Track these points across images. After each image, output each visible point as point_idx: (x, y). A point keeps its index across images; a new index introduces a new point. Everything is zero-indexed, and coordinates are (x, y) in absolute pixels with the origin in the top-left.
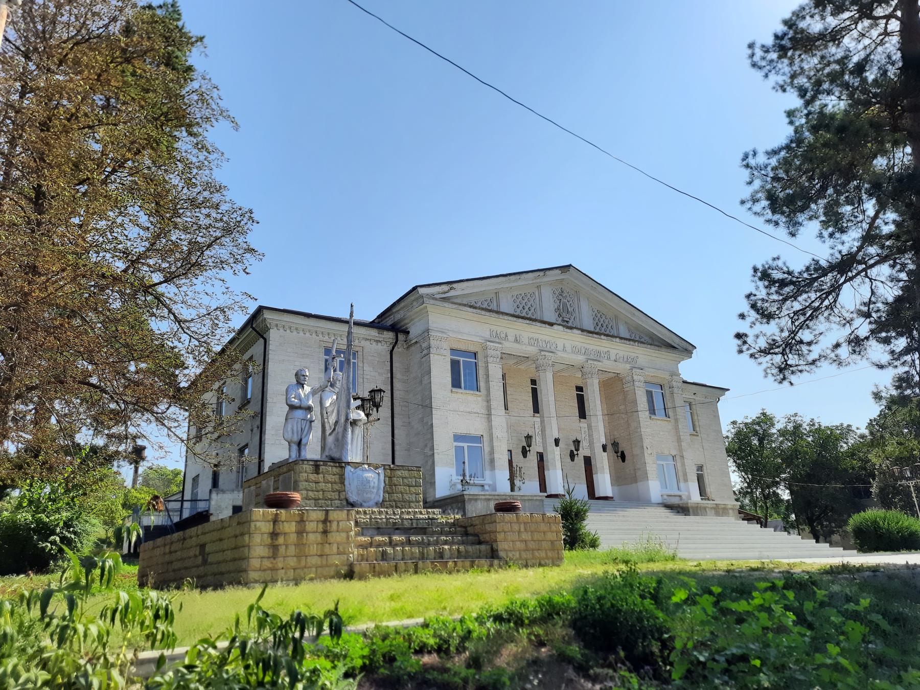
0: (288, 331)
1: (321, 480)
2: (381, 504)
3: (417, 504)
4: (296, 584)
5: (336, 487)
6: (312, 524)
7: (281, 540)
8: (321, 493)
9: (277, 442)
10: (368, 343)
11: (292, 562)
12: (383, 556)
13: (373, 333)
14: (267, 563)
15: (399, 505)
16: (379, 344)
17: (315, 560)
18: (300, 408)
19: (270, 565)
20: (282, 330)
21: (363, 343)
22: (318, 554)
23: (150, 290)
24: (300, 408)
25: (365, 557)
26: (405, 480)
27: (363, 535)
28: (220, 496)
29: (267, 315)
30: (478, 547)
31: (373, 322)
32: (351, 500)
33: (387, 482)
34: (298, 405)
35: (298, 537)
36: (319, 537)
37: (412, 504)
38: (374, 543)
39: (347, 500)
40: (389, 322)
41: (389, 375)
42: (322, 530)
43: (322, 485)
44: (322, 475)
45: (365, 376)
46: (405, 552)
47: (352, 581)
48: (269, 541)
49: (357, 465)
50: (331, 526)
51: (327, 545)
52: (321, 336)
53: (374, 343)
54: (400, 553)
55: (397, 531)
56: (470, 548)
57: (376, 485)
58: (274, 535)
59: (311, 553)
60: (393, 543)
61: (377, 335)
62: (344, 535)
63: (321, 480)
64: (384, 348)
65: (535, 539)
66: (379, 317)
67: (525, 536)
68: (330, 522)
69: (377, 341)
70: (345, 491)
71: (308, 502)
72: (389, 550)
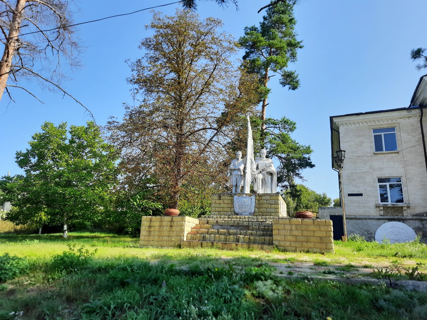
0: (349, 125)
1: (222, 203)
2: (254, 214)
3: (276, 214)
4: (161, 248)
5: (229, 206)
6: (165, 222)
7: (152, 229)
8: (222, 208)
9: (349, 183)
10: (402, 120)
11: (156, 238)
12: (203, 238)
13: (405, 113)
14: (146, 238)
15: (264, 214)
16: (411, 118)
17: (165, 238)
18: (234, 170)
19: (148, 239)
20: (345, 126)
21: (399, 121)
22: (168, 235)
23: (216, 131)
24: (234, 170)
25: (195, 238)
26: (268, 201)
27: (213, 228)
28: (323, 210)
29: (335, 120)
30: (263, 237)
31: (410, 106)
32: (236, 212)
33: (257, 203)
34: (233, 169)
35: (159, 228)
36: (168, 228)
37: (272, 214)
38: (209, 233)
39: (234, 212)
40: (418, 103)
41: (421, 136)
42: (170, 225)
43: (222, 205)
44: (222, 201)
45: (402, 140)
46: (216, 238)
47: (213, 249)
48: (148, 229)
49: (240, 195)
50: (173, 224)
51: (172, 232)
52: (369, 123)
53: (407, 119)
54: (213, 238)
55: (232, 227)
56: (257, 238)
57: (250, 204)
58: (150, 227)
59: (165, 235)
60: (219, 233)
61: (407, 113)
62: (179, 228)
63: (222, 203)
64: (415, 120)
65: (304, 235)
66: (412, 101)
67: (295, 233)
68: (174, 222)
69: (409, 117)
70: (234, 207)
71: (215, 213)
72: (207, 236)
